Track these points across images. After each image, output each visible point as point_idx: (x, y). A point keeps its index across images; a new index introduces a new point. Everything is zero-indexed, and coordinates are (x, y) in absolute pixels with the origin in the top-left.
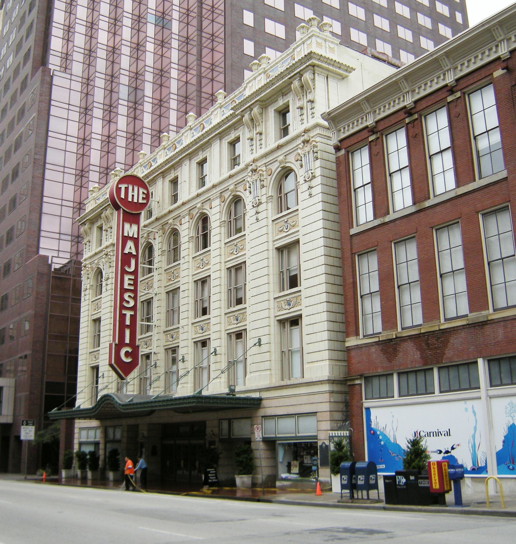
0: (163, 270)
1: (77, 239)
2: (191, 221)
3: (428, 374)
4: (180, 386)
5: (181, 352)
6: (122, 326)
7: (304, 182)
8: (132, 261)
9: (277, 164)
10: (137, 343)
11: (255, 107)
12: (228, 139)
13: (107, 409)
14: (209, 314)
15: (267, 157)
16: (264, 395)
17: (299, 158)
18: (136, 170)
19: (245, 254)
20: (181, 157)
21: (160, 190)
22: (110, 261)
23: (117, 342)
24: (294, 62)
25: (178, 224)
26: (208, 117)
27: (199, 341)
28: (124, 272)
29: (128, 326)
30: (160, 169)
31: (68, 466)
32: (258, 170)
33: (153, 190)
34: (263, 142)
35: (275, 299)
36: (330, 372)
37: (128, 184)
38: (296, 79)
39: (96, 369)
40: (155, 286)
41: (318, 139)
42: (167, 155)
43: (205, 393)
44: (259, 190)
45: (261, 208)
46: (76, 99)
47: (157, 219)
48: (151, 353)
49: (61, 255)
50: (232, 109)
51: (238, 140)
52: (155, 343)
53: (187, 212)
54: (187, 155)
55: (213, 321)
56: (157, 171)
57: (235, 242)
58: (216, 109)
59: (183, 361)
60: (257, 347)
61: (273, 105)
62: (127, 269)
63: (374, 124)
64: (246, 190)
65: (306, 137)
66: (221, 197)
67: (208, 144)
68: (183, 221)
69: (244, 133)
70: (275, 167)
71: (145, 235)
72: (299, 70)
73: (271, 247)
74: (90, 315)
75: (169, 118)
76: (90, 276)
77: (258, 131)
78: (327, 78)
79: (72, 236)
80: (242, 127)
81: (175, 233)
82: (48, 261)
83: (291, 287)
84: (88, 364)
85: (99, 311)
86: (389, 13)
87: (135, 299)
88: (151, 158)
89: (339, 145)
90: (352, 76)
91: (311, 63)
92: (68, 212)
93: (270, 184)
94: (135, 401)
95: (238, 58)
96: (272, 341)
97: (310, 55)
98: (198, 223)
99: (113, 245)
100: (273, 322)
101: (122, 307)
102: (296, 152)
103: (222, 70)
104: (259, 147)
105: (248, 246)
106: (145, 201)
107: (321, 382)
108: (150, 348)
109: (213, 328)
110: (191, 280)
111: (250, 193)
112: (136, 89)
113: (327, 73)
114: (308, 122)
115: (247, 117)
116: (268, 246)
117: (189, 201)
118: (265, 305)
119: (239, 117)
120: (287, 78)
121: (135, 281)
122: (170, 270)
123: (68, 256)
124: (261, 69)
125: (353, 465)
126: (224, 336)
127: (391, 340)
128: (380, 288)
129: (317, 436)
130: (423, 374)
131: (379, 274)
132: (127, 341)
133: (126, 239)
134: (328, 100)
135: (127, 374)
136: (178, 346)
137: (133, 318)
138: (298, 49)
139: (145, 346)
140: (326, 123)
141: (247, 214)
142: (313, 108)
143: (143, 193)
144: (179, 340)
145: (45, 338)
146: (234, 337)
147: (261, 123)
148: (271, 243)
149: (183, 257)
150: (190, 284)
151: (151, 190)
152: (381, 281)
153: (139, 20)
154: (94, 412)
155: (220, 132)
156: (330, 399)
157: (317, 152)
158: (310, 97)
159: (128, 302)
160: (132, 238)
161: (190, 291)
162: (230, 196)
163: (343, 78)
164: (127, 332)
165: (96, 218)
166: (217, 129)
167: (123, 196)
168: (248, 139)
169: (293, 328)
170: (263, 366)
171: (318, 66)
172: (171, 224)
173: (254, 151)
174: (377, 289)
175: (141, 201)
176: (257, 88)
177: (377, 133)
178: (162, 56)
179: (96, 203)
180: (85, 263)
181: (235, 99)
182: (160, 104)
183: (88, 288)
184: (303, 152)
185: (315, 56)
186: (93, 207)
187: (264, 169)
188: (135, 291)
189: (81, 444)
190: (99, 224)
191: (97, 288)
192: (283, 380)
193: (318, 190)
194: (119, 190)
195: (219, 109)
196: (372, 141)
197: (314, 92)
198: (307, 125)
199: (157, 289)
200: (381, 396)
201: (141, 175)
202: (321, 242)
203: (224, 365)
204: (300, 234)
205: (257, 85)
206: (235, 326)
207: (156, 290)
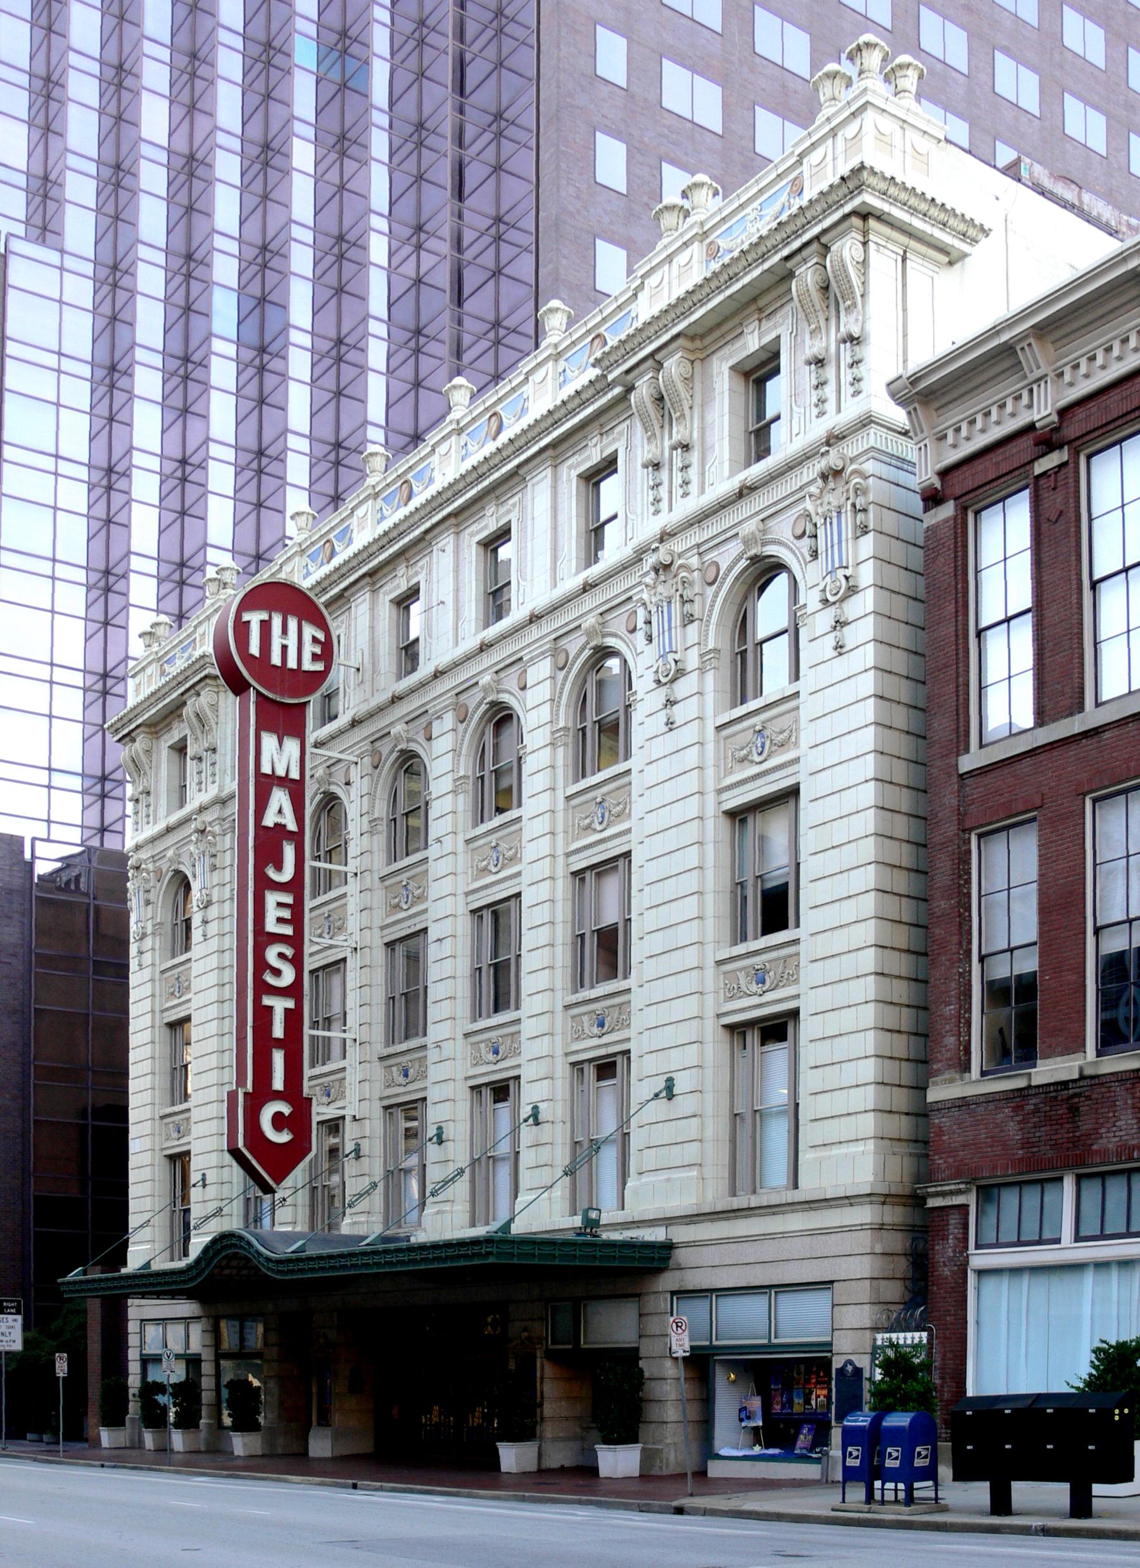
0: (376, 877)
1: (101, 786)
2: (461, 727)
3: (1050, 1189)
4: (429, 1210)
5: (434, 1115)
6: (264, 1044)
7: (820, 606)
8: (282, 851)
9: (734, 548)
10: (306, 1092)
11: (671, 354)
12: (579, 464)
13: (227, 1272)
14: (425, 1035)
15: (704, 524)
16: (680, 1234)
17: (809, 529)
18: (287, 569)
19: (629, 831)
20: (428, 525)
21: (363, 628)
22: (213, 851)
23: (249, 1087)
24: (798, 203)
25: (421, 738)
26: (513, 389)
27: (487, 1085)
28: (264, 884)
29: (279, 1043)
30: (363, 562)
31: (114, 1417)
32: (674, 568)
33: (341, 631)
34: (693, 474)
35: (719, 963)
36: (875, 1174)
37: (270, 609)
38: (805, 261)
39: (179, 1161)
40: (353, 923)
41: (870, 467)
42: (383, 518)
43: (516, 1229)
44: (677, 632)
45: (683, 687)
46: (80, 334)
47: (355, 723)
48: (343, 1118)
49: (57, 832)
50: (597, 363)
51: (608, 466)
52: (353, 1092)
53: (448, 699)
54: (449, 516)
55: (529, 1028)
56: (353, 570)
57: (598, 794)
58: (539, 365)
59: (440, 1142)
60: (663, 1103)
61: (726, 351)
62: (271, 873)
63: (1055, 418)
64: (633, 630)
65: (833, 459)
66: (555, 652)
67: (516, 480)
68: (436, 730)
69: (632, 443)
70: (730, 558)
71: (320, 772)
72: (816, 230)
73: (711, 810)
74: (157, 1010)
75: (363, 402)
76: (152, 896)
77: (676, 437)
78: (904, 259)
79: (83, 775)
80: (624, 425)
81: (409, 764)
82: (22, 852)
83: (767, 929)
84: (157, 1148)
85: (183, 999)
86: (1045, 52)
87: (297, 962)
88: (332, 529)
89: (938, 485)
90: (980, 254)
91: (855, 206)
92: (71, 703)
93: (711, 611)
94: (311, 1252)
95: (578, 197)
96: (709, 1086)
97: (855, 179)
98: (483, 733)
99: (222, 802)
100: (712, 1031)
101: (263, 988)
102: (798, 509)
103: (528, 240)
104: (680, 492)
105: (638, 807)
106: (319, 667)
107: (849, 1200)
108: (339, 1104)
109: (529, 1050)
110: (461, 908)
111: (650, 639)
112: (262, 303)
113: (904, 239)
114: (839, 410)
115: (643, 389)
116: (703, 806)
117: (456, 665)
118: (687, 983)
119: (617, 390)
120: (777, 258)
121: (297, 909)
122: (398, 879)
123: (75, 835)
124: (692, 226)
125: (876, 1422)
126: (562, 1069)
127: (1064, 1084)
128: (1041, 933)
129: (830, 1344)
130: (1122, 1181)
131: (1042, 893)
132: (278, 1084)
133: (266, 784)
134: (905, 336)
135: (279, 1178)
136: (424, 1099)
137: (293, 1018)
138: (815, 157)
139: (325, 1100)
140: (899, 416)
141: (638, 706)
142: (858, 362)
143: (315, 640)
144: (521, 1060)
145: (25, 1075)
146: (590, 1072)
147: (687, 411)
148: (711, 798)
149: (438, 840)
150: (460, 920)
151: (337, 627)
152: (1044, 911)
153: (267, 57)
154: (192, 1279)
155: (556, 439)
156: (872, 1248)
157: (865, 510)
158: (850, 324)
159: (277, 973)
160: (284, 781)
161: (460, 940)
162: (583, 649)
163: (953, 259)
164: (278, 1058)
165: (166, 717)
166: (547, 431)
167: (254, 649)
168: (645, 466)
169: (766, 1048)
170: (677, 1155)
171: (880, 217)
172: (398, 738)
173: (664, 505)
174: (1032, 935)
175: (308, 665)
176: (680, 292)
177: (1060, 447)
178: (342, 187)
179: (163, 673)
180: (135, 857)
181: (602, 330)
182: (338, 352)
183: (149, 930)
184: (820, 510)
185: (872, 181)
186: (153, 688)
187: (694, 561)
188: (296, 941)
189: (147, 1361)
190: (176, 739)
191: (173, 930)
192: (733, 1194)
193: (863, 631)
194: (242, 629)
195: (550, 364)
196: (1044, 474)
197: (863, 306)
198: (833, 421)
199: (357, 936)
200: (1022, 1239)
201: (305, 584)
202: (868, 794)
203: (562, 1156)
204: (803, 768)
205: (675, 282)
206: (596, 1042)
207: (355, 939)
